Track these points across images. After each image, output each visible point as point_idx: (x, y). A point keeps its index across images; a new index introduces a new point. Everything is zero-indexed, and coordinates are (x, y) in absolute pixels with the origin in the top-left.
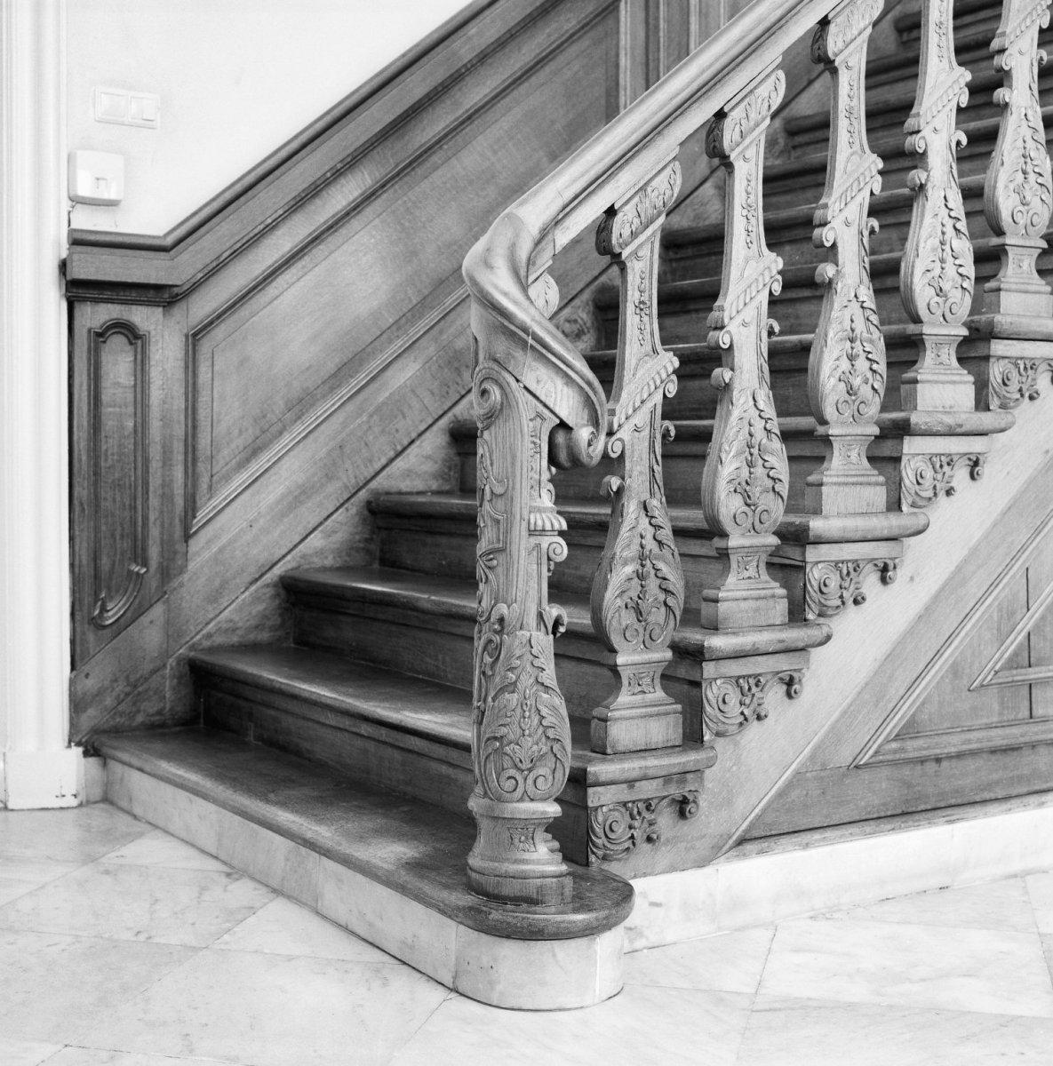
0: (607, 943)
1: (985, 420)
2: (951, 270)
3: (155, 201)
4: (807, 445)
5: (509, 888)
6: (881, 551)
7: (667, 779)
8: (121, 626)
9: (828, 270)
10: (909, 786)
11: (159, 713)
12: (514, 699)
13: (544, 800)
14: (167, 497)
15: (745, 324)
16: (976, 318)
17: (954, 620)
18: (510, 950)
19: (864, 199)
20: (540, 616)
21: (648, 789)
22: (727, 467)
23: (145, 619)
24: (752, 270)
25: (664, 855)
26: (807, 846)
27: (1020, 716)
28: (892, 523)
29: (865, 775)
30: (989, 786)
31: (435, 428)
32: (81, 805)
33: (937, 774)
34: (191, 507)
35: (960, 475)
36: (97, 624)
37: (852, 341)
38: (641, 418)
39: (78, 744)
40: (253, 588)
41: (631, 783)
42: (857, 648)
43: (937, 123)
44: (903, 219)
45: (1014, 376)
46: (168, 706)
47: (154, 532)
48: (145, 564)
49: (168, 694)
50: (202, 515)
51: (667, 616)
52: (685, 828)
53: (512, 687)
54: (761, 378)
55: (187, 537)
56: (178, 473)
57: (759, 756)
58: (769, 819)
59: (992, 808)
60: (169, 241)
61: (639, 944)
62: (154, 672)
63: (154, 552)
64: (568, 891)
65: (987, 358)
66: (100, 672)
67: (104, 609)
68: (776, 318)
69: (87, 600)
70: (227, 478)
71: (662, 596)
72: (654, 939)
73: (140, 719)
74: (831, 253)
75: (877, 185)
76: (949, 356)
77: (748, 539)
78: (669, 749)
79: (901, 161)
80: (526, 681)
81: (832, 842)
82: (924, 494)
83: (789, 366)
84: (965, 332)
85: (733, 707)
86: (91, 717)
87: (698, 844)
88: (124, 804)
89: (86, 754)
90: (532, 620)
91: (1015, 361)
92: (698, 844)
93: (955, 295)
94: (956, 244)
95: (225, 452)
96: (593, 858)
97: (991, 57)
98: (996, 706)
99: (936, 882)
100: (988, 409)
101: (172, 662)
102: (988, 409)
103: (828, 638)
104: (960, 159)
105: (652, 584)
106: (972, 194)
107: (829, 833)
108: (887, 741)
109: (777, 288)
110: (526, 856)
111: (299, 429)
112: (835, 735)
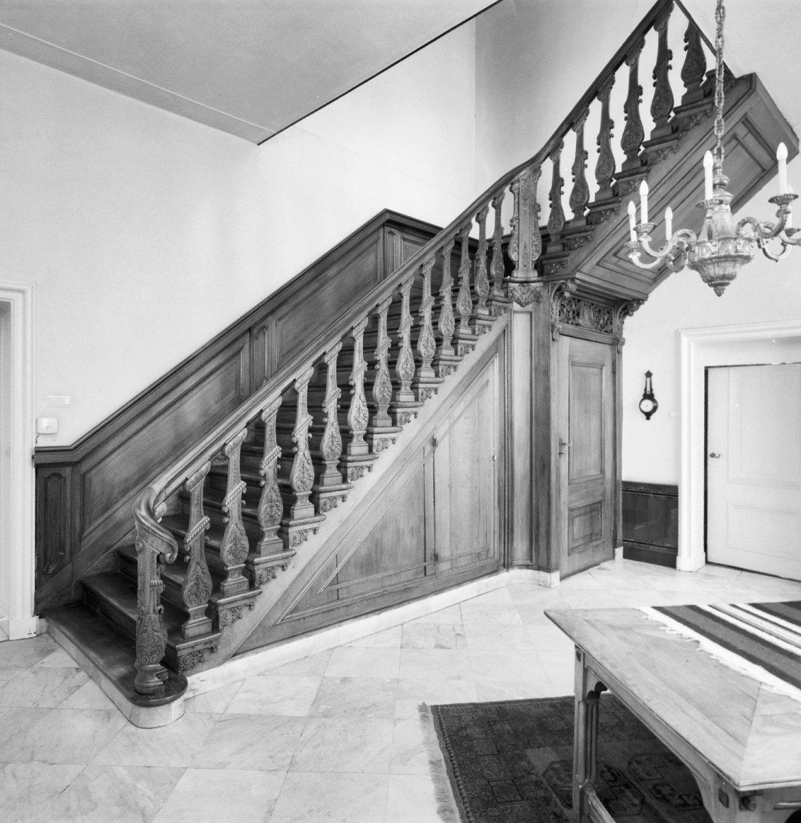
0: (176, 706)
1: (438, 379)
2: (306, 475)
3: (68, 433)
4: (396, 385)
5: (144, 691)
6: (281, 562)
7: (206, 643)
8: (54, 573)
9: (325, 420)
10: (294, 627)
11: (69, 600)
12: (145, 635)
13: (155, 663)
14: (72, 527)
15: (233, 504)
16: (393, 402)
17: (310, 575)
18: (144, 711)
19: (306, 428)
20: (154, 610)
21: (200, 647)
22: (377, 390)
23: (64, 570)
24: (361, 365)
25: (206, 665)
26: (257, 653)
27: (335, 599)
28: (455, 358)
29: (279, 627)
30: (323, 623)
31: (174, 494)
32: (38, 636)
33: (304, 622)
34: (83, 529)
35: (452, 370)
36: (45, 574)
37: (271, 502)
38: (272, 464)
39: (37, 615)
40: (105, 554)
41: (193, 647)
42: (272, 591)
43: (302, 433)
44: (320, 434)
45: (425, 393)
46: (72, 597)
47: (68, 540)
48: (64, 551)
49: (74, 594)
50: (86, 533)
51: (206, 595)
52: (213, 655)
53: (145, 631)
54: (239, 519)
55: (81, 540)
56: (78, 520)
57: (239, 629)
58: (245, 646)
59: (322, 630)
60: (72, 447)
61: (196, 694)
62: (68, 586)
63: (68, 548)
64: (163, 690)
65: (475, 324)
66: (47, 588)
67: (48, 568)
68: (245, 500)
69: (42, 566)
70: (96, 519)
71: (204, 589)
72: (202, 691)
73: (61, 603)
74: (296, 444)
75: (433, 304)
76: (429, 365)
77: (302, 493)
78: (206, 634)
79: (372, 365)
80: (149, 629)
81: (266, 650)
82: (296, 542)
83: (314, 445)
84: (311, 492)
85: (230, 617)
86: (43, 604)
87: (218, 659)
88: (52, 635)
89: (40, 618)
90: (152, 611)
91: (328, 498)
92: (218, 659)
93: (363, 422)
94: (308, 467)
95: (95, 510)
96: (180, 671)
97: (397, 333)
98: (326, 598)
99: (303, 655)
100: (439, 377)
101: (74, 583)
102: (439, 377)
103: (261, 593)
104: (338, 412)
105: (201, 586)
106: (454, 306)
107: (265, 648)
108: (287, 615)
109: (390, 347)
110: (150, 681)
111: (124, 500)
112: (268, 616)
